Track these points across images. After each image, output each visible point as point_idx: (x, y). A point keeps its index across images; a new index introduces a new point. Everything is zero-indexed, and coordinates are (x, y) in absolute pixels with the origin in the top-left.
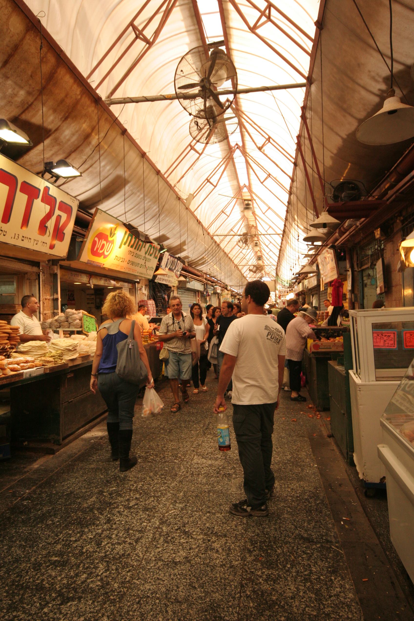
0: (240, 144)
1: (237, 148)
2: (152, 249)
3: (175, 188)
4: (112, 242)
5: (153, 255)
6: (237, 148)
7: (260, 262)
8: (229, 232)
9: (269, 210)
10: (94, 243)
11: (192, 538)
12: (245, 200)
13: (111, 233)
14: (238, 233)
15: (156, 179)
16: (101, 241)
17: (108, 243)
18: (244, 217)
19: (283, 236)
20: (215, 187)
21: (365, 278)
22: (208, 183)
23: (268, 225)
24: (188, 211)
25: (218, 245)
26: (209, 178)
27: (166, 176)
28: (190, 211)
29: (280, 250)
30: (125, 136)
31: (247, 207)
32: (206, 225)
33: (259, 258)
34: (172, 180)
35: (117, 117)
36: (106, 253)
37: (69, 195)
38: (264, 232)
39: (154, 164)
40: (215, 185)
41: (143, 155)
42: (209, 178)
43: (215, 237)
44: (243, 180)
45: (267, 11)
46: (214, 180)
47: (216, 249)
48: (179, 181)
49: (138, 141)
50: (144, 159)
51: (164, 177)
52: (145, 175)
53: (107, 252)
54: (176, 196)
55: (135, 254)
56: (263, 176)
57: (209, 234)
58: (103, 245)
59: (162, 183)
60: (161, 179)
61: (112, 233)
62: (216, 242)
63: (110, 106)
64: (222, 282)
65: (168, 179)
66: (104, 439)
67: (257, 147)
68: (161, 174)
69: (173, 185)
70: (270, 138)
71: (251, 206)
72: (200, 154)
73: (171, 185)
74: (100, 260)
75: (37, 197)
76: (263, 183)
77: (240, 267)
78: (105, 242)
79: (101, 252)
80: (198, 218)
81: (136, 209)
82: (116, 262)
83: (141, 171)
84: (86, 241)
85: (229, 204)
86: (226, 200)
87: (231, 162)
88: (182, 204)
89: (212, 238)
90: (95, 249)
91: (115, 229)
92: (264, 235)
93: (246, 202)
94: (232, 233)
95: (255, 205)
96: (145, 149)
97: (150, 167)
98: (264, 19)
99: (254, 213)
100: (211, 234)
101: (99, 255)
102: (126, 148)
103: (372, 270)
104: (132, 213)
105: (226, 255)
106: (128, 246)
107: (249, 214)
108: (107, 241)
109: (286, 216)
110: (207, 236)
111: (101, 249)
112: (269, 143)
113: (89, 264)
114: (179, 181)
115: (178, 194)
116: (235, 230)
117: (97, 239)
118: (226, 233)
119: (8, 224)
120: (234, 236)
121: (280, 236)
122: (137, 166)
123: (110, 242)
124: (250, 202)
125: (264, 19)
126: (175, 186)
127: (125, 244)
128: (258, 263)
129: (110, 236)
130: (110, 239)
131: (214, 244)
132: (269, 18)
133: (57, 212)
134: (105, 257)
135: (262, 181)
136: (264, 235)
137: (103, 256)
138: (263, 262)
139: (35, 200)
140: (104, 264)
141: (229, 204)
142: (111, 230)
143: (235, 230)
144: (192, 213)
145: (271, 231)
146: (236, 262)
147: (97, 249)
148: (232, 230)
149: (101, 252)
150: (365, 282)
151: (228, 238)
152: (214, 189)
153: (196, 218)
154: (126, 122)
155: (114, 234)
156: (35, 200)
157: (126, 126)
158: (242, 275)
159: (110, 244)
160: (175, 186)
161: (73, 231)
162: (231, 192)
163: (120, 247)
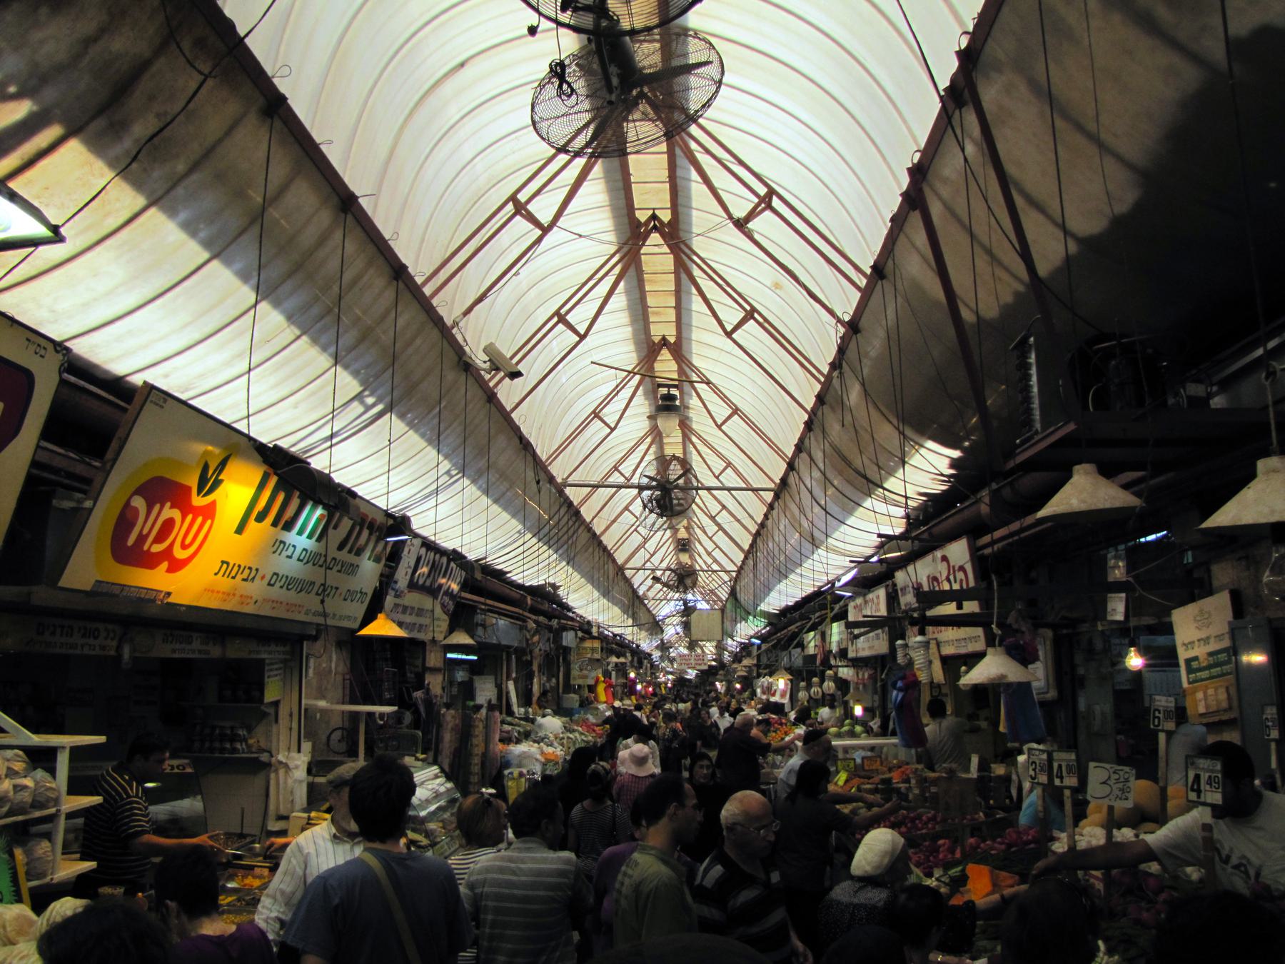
0: (665, 216)
2: (366, 533)
3: (454, 331)
4: (209, 512)
7: (685, 558)
8: (608, 475)
9: (736, 416)
10: (125, 521)
12: (660, 385)
13: (203, 481)
14: (635, 480)
15: (390, 294)
16: (157, 507)
17: (190, 517)
18: (656, 435)
19: (777, 496)
20: (582, 337)
21: (1079, 658)
22: (561, 326)
24: (493, 408)
25: (577, 513)
26: (563, 311)
27: (427, 290)
28: (500, 407)
29: (757, 535)
30: (276, 118)
31: (667, 405)
32: (542, 452)
33: (684, 546)
34: (448, 306)
35: (242, 34)
36: (180, 554)
37: (15, 326)
38: (710, 481)
39: (385, 242)
40: (582, 332)
41: (346, 203)
42: (563, 311)
43: (568, 491)
44: (663, 328)
46: (579, 317)
47: (571, 523)
48: (468, 312)
49: (334, 155)
50: (350, 217)
51: (423, 294)
52: (348, 276)
53: (184, 547)
54: (456, 358)
56: (721, 411)
57: (551, 479)
58: (169, 524)
59: (409, 315)
60: (408, 296)
61: (208, 482)
62: (570, 504)
64: (577, 615)
65: (435, 302)
67: (730, 217)
68: (411, 278)
69: (449, 322)
70: (771, 192)
71: (678, 403)
72: (546, 230)
73: (441, 318)
74: (156, 580)
76: (724, 427)
77: (628, 573)
78: (176, 514)
79: (157, 548)
80: (524, 430)
81: (313, 393)
82: (225, 583)
83: (334, 264)
84: (90, 510)
85: (617, 391)
86: (608, 381)
87: (632, 271)
88: (1080, 140)
89: (561, 492)
90: (131, 542)
91: (223, 465)
93: (664, 391)
94: (616, 478)
95: (694, 402)
96: (357, 180)
97: (371, 249)
99: (685, 426)
100: (559, 480)
101: (150, 561)
102: (279, 171)
103: (332, 361)
104: (296, 406)
105: (595, 539)
106: (275, 524)
107: (670, 426)
108: (186, 508)
109: (801, 440)
110: (545, 486)
111: (158, 539)
112: (768, 213)
113: (102, 591)
114: (468, 312)
115: (464, 352)
116: (626, 468)
117: (139, 503)
118: (595, 479)
120: (620, 487)
121: (761, 499)
122: (323, 239)
123: (197, 511)
124: (674, 392)
126: (456, 324)
127: (260, 518)
128: (679, 563)
129: (199, 493)
131: (563, 511)
132: (769, 207)
134: (176, 566)
135: (719, 422)
136: (709, 489)
137: (165, 565)
138: (692, 557)
140: (169, 594)
141: (617, 391)
142: (206, 468)
143: (626, 468)
144: (506, 416)
145: (730, 479)
146: (620, 557)
147: (142, 538)
148: (616, 468)
149: (157, 548)
150: (1081, 671)
151: (604, 493)
152: (609, 435)
153: (516, 430)
154: (286, 71)
155: (217, 483)
157: (283, 86)
158: (635, 592)
159: (200, 520)
160: (456, 324)
161: (35, 464)
162: (628, 356)
163: (240, 530)
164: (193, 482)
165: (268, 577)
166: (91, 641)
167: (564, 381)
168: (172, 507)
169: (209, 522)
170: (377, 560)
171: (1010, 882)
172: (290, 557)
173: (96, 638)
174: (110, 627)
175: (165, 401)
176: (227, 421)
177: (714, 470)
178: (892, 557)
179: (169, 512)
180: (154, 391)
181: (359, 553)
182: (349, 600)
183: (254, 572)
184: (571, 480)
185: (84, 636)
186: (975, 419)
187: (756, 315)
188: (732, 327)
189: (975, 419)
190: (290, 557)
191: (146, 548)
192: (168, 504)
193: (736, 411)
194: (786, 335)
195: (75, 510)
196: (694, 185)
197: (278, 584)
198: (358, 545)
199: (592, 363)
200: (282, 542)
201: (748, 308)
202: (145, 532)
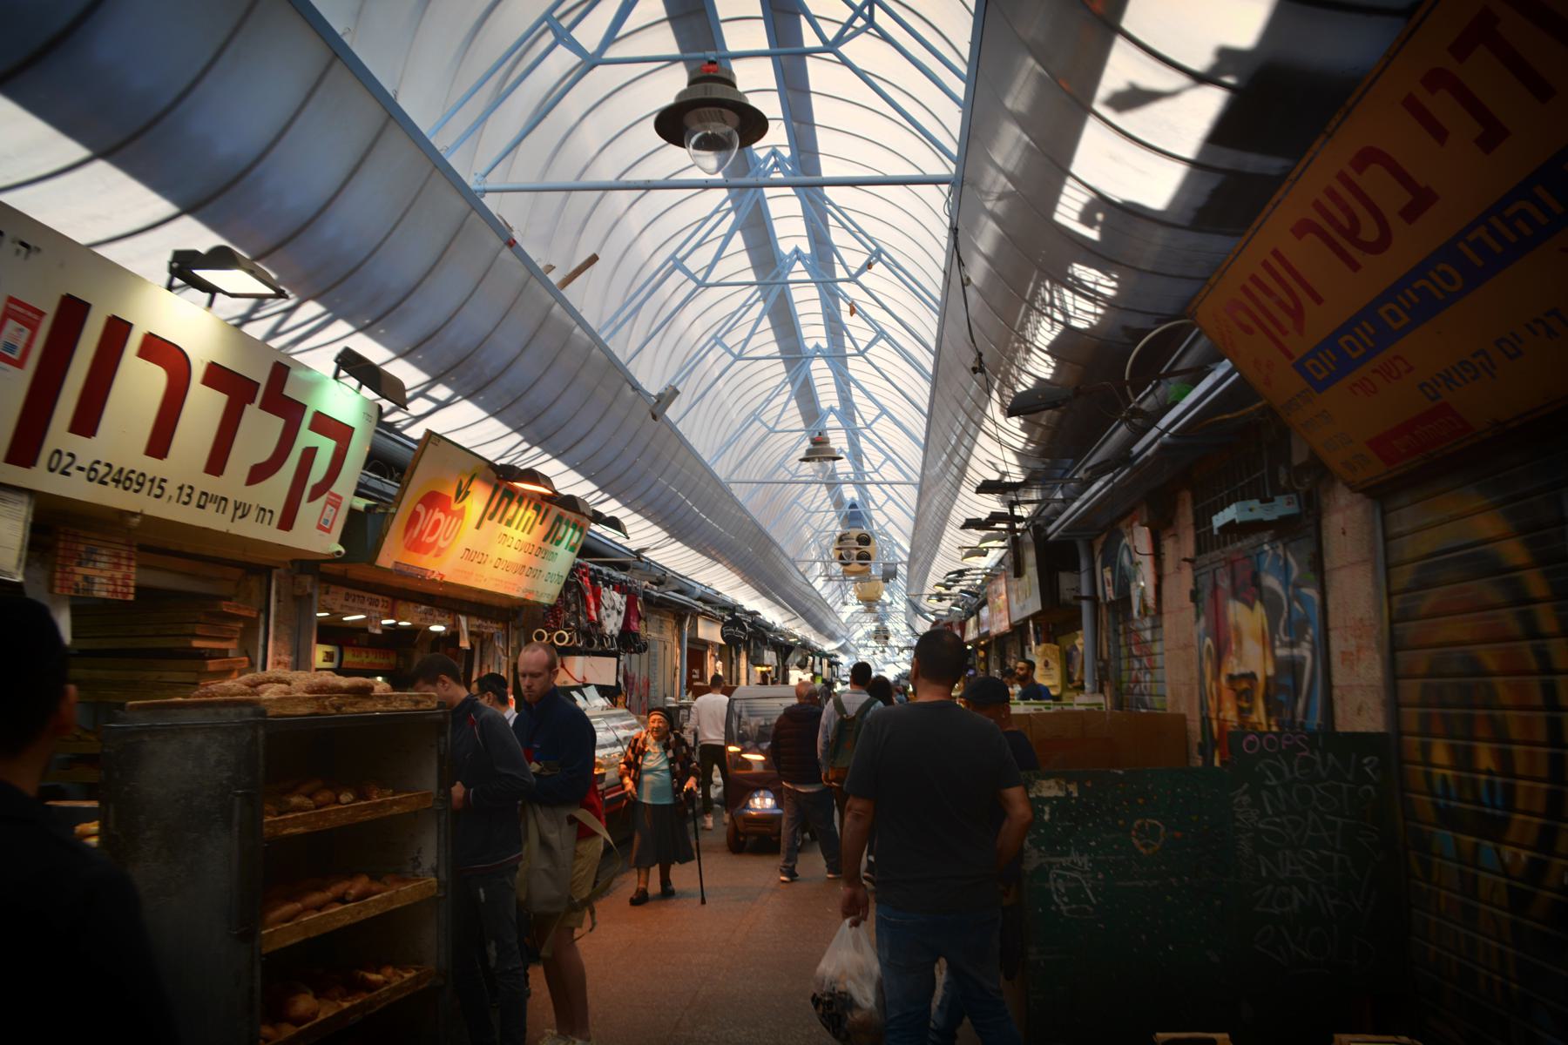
1: (776, 164)
4: (461, 514)
5: (210, 496)
6: (799, 259)
11: (870, 602)
16: (431, 511)
17: (450, 517)
23: (887, 494)
42: (719, 335)
45: (866, 11)
53: (445, 539)
55: (195, 496)
58: (437, 523)
61: (462, 494)
63: (483, 196)
66: (855, 615)
75: (252, 401)
78: (441, 516)
84: (394, 514)
92: (878, 484)
98: (860, 22)
113: (400, 571)
117: (421, 509)
119: (222, 477)
123: (453, 514)
125: (860, 22)
129: (457, 498)
130: (456, 507)
132: (870, 21)
133: (307, 437)
139: (248, 406)
147: (421, 533)
155: (467, 493)
156: (248, 406)
163: (478, 527)
164: (452, 493)
165: (494, 561)
166: (374, 608)
167: (730, 406)
168: (440, 511)
169: (460, 521)
170: (572, 549)
171: (1015, 607)
172: (509, 546)
173: (377, 606)
174: (386, 599)
175: (439, 441)
176: (466, 445)
177: (873, 462)
178: (353, 621)
179: (439, 515)
180: (27, 331)
181: (558, 543)
182: (549, 582)
183: (485, 556)
184: (734, 478)
185: (370, 604)
186: (482, 895)
187: (883, 256)
188: (856, 270)
189: (482, 895)
190: (509, 546)
191: (423, 539)
192: (437, 509)
193: (890, 520)
194: (929, 289)
195: (385, 514)
196: (836, 266)
197: (500, 567)
198: (557, 537)
199: (593, 259)
200: (505, 535)
201: (874, 248)
202: (423, 528)
